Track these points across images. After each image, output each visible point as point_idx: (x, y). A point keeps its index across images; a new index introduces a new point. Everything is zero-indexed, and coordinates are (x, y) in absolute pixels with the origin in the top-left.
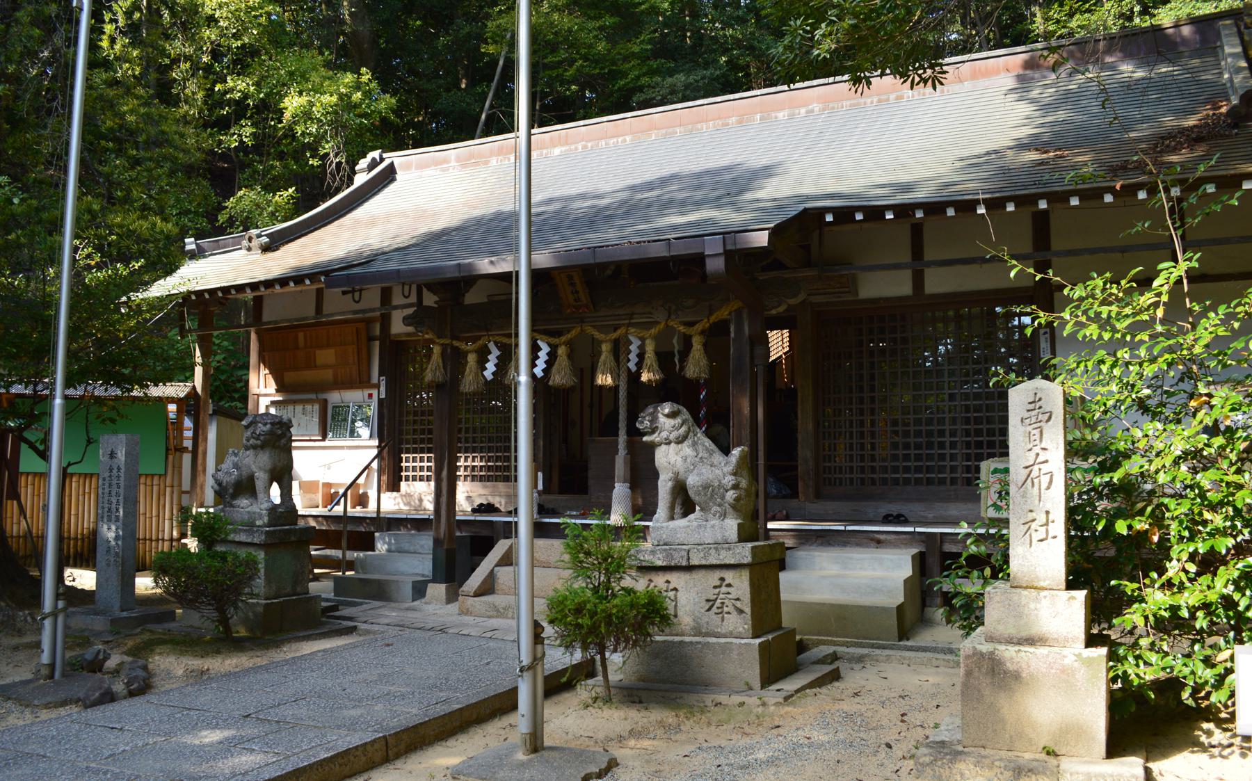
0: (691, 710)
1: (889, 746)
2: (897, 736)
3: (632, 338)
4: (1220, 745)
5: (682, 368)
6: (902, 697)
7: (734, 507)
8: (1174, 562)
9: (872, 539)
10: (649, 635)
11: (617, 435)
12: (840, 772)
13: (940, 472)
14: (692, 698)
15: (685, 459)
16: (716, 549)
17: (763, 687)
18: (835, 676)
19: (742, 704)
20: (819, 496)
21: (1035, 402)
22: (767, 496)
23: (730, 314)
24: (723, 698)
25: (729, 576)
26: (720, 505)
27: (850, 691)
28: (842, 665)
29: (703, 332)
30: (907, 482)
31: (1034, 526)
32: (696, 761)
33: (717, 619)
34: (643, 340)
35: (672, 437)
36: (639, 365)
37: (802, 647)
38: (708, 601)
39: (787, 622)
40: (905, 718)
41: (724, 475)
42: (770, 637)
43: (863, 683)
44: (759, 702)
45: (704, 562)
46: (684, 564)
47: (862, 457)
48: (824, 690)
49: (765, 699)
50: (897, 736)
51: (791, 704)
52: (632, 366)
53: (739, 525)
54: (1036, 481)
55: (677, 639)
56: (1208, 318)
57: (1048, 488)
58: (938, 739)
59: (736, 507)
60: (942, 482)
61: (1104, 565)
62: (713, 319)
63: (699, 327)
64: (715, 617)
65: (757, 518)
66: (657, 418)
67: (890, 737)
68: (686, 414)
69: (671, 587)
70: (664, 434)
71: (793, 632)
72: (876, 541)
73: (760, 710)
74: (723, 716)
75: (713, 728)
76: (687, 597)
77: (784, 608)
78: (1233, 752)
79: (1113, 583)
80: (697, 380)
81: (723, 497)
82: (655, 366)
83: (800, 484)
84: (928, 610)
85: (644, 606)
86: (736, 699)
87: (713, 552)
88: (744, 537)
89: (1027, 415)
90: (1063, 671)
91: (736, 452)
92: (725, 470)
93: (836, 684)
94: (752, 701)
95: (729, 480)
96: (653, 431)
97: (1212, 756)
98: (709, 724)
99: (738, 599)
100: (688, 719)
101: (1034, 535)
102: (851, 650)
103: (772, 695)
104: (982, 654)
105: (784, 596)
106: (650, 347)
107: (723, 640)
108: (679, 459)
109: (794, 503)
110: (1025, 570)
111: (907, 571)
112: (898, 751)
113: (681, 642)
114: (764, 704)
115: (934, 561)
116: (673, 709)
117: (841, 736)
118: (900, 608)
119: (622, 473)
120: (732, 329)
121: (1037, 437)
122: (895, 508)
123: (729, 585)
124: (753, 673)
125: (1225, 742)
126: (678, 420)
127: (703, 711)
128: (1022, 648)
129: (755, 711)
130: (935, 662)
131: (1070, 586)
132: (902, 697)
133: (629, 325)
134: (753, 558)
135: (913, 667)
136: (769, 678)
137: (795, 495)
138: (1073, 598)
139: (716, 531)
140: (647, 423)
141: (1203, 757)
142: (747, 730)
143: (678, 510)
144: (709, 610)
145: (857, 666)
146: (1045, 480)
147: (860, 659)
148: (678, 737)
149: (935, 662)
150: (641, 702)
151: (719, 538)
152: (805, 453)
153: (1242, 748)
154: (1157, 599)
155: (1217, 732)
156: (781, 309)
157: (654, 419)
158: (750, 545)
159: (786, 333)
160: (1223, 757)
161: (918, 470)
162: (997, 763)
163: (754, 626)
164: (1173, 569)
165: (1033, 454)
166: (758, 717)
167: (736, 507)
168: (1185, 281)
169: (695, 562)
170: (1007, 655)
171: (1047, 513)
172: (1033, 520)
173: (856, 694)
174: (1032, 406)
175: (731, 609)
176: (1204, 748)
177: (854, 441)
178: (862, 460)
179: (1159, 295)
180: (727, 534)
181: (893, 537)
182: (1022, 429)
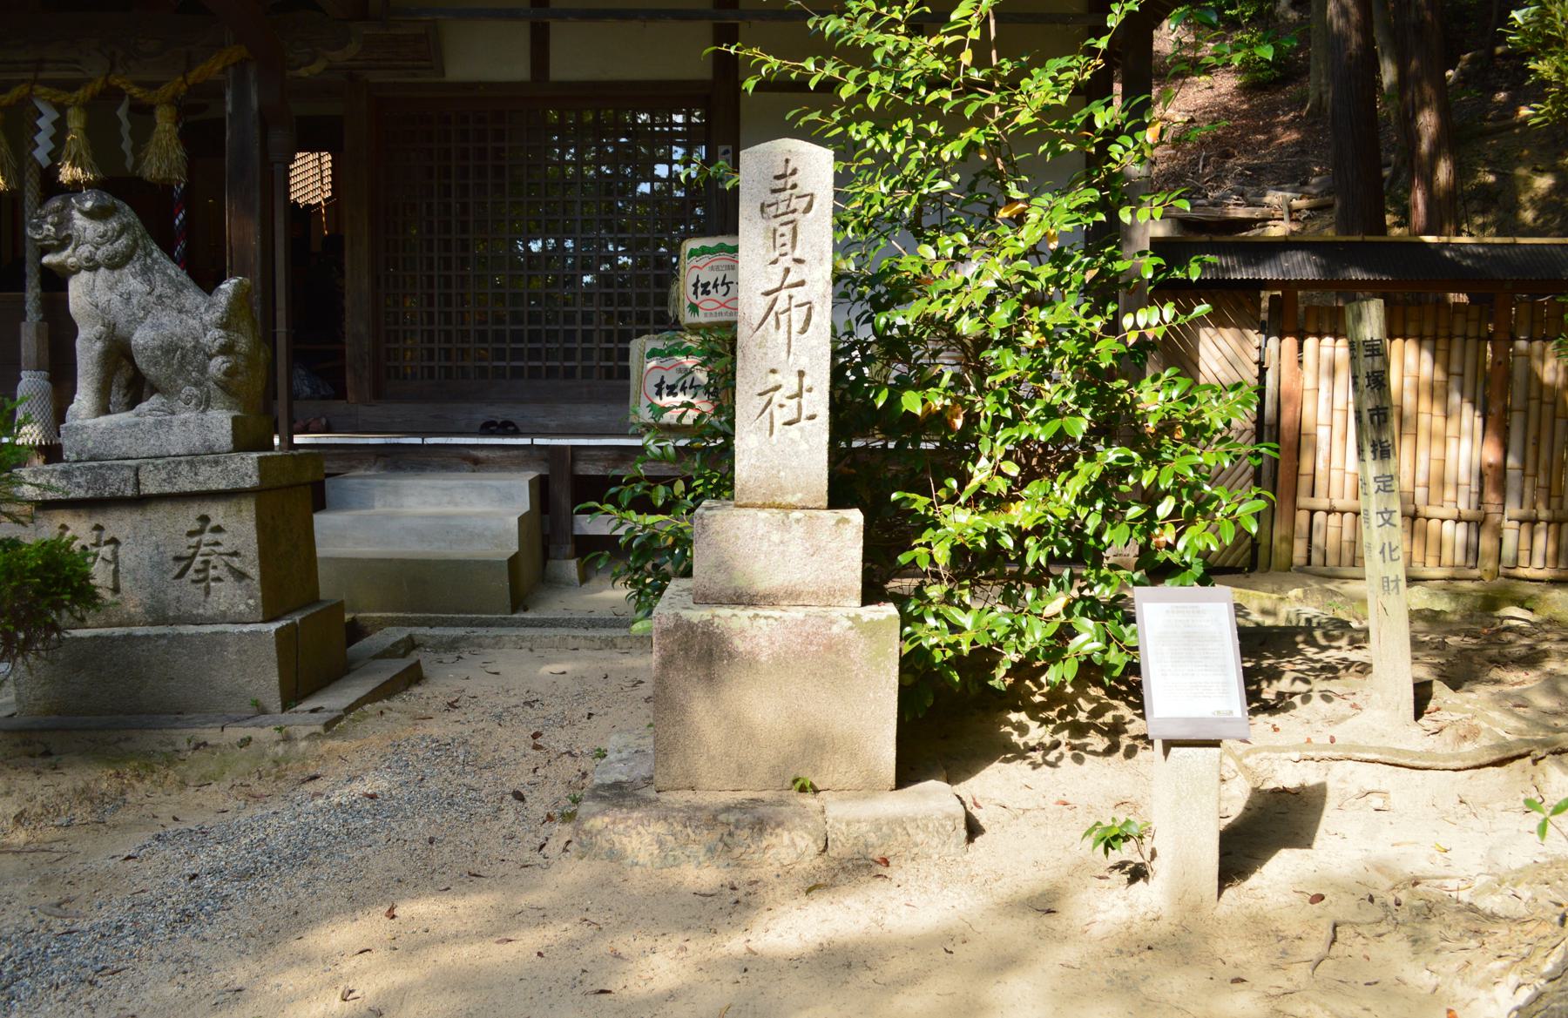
0: (148, 763)
1: (519, 796)
2: (531, 777)
3: (41, 106)
4: (1041, 745)
5: (138, 163)
6: (529, 704)
7: (224, 387)
8: (983, 462)
9: (466, 458)
10: (54, 627)
11: (23, 289)
12: (437, 862)
13: (566, 359)
14: (150, 740)
15: (127, 298)
16: (191, 464)
17: (286, 706)
18: (414, 676)
19: (246, 742)
20: (378, 394)
21: (784, 178)
22: (293, 396)
23: (224, 70)
24: (210, 734)
25: (218, 513)
26: (197, 384)
27: (441, 701)
28: (424, 658)
29: (173, 101)
30: (517, 373)
31: (778, 397)
32: (149, 868)
33: (197, 591)
34: (61, 108)
35: (99, 255)
36: (55, 157)
37: (356, 631)
38: (178, 559)
39: (327, 590)
40: (540, 741)
41: (205, 329)
42: (297, 618)
43: (462, 684)
44: (277, 736)
45: (167, 489)
46: (129, 492)
47: (448, 334)
48: (396, 703)
49: (291, 729)
50: (531, 777)
51: (342, 734)
52: (41, 155)
53: (235, 420)
54: (783, 318)
55: (118, 631)
56: (1031, 77)
57: (803, 331)
58: (609, 779)
59: (229, 387)
60: (570, 373)
61: (882, 465)
62: (192, 77)
63: (167, 91)
64: (192, 588)
65: (275, 397)
66: (70, 219)
67: (521, 780)
68: (128, 215)
69: (105, 537)
70: (85, 250)
71: (339, 607)
72: (471, 461)
73: (280, 749)
74: (213, 767)
75: (191, 791)
76: (127, 558)
77: (322, 571)
78: (1061, 756)
79: (894, 496)
80: (167, 187)
81: (203, 369)
82: (86, 158)
83: (348, 376)
84: (551, 563)
85: (34, 572)
86: (235, 733)
87: (184, 469)
88: (242, 442)
89: (771, 198)
90: (829, 647)
91: (228, 286)
92: (207, 318)
93: (416, 690)
94: (264, 734)
95: (214, 338)
96: (63, 244)
97: (1035, 766)
98: (183, 784)
99: (235, 554)
100: (141, 779)
101: (777, 413)
102: (437, 631)
103: (303, 721)
104: (691, 626)
105: (322, 551)
106: (75, 122)
107: (208, 629)
108: (116, 299)
109: (338, 406)
110: (762, 475)
111: (523, 504)
112: (538, 806)
113: (128, 638)
114: (288, 739)
115: (563, 490)
116: (110, 763)
117: (432, 785)
118: (513, 560)
119: (33, 356)
120: (228, 98)
121: (788, 238)
122: (499, 413)
123: (218, 529)
124: (267, 685)
125: (1047, 740)
126: (114, 224)
127: (171, 760)
128: (761, 612)
129: (270, 752)
130: (572, 643)
131: (838, 498)
132: (529, 704)
133: (36, 81)
134: (262, 477)
135: (537, 652)
136: (296, 690)
137: (341, 394)
138: (845, 521)
139: (192, 430)
140: (49, 228)
141: (1019, 769)
142: (258, 788)
143: (117, 396)
144: (181, 575)
145: (449, 657)
146: (798, 316)
147: (453, 645)
148: (120, 817)
149: (572, 643)
150: (47, 754)
151: (197, 441)
152: (356, 326)
153: (1073, 748)
154: (960, 522)
155: (1033, 725)
156: (317, 68)
157: (64, 222)
158: (255, 455)
159: (327, 157)
160: (1053, 765)
161: (535, 354)
162: (723, 817)
163: (266, 600)
164: (980, 472)
165: (778, 270)
166: (276, 763)
167: (229, 387)
168: (992, 22)
169: (150, 488)
170: (735, 624)
171: (801, 374)
172: (777, 388)
173: (452, 705)
174: (780, 184)
175: (221, 571)
176: (1020, 753)
177: (436, 309)
178: (448, 339)
179: (964, 31)
180: (212, 437)
181: (499, 453)
182: (761, 224)
